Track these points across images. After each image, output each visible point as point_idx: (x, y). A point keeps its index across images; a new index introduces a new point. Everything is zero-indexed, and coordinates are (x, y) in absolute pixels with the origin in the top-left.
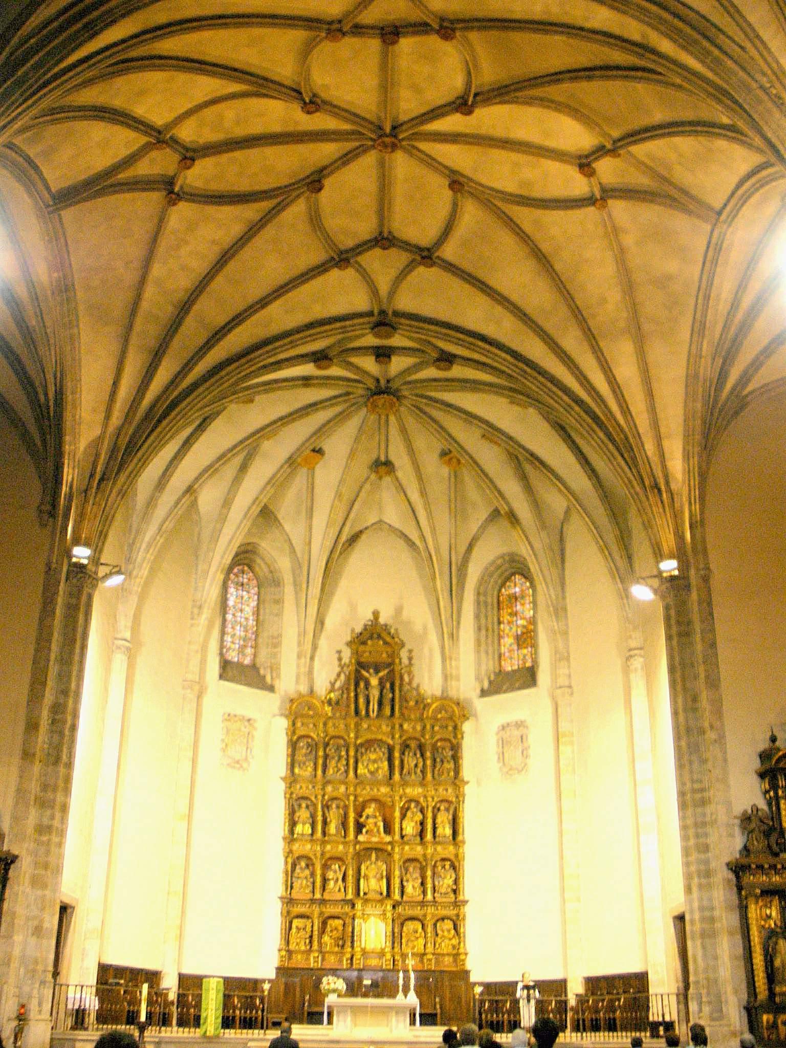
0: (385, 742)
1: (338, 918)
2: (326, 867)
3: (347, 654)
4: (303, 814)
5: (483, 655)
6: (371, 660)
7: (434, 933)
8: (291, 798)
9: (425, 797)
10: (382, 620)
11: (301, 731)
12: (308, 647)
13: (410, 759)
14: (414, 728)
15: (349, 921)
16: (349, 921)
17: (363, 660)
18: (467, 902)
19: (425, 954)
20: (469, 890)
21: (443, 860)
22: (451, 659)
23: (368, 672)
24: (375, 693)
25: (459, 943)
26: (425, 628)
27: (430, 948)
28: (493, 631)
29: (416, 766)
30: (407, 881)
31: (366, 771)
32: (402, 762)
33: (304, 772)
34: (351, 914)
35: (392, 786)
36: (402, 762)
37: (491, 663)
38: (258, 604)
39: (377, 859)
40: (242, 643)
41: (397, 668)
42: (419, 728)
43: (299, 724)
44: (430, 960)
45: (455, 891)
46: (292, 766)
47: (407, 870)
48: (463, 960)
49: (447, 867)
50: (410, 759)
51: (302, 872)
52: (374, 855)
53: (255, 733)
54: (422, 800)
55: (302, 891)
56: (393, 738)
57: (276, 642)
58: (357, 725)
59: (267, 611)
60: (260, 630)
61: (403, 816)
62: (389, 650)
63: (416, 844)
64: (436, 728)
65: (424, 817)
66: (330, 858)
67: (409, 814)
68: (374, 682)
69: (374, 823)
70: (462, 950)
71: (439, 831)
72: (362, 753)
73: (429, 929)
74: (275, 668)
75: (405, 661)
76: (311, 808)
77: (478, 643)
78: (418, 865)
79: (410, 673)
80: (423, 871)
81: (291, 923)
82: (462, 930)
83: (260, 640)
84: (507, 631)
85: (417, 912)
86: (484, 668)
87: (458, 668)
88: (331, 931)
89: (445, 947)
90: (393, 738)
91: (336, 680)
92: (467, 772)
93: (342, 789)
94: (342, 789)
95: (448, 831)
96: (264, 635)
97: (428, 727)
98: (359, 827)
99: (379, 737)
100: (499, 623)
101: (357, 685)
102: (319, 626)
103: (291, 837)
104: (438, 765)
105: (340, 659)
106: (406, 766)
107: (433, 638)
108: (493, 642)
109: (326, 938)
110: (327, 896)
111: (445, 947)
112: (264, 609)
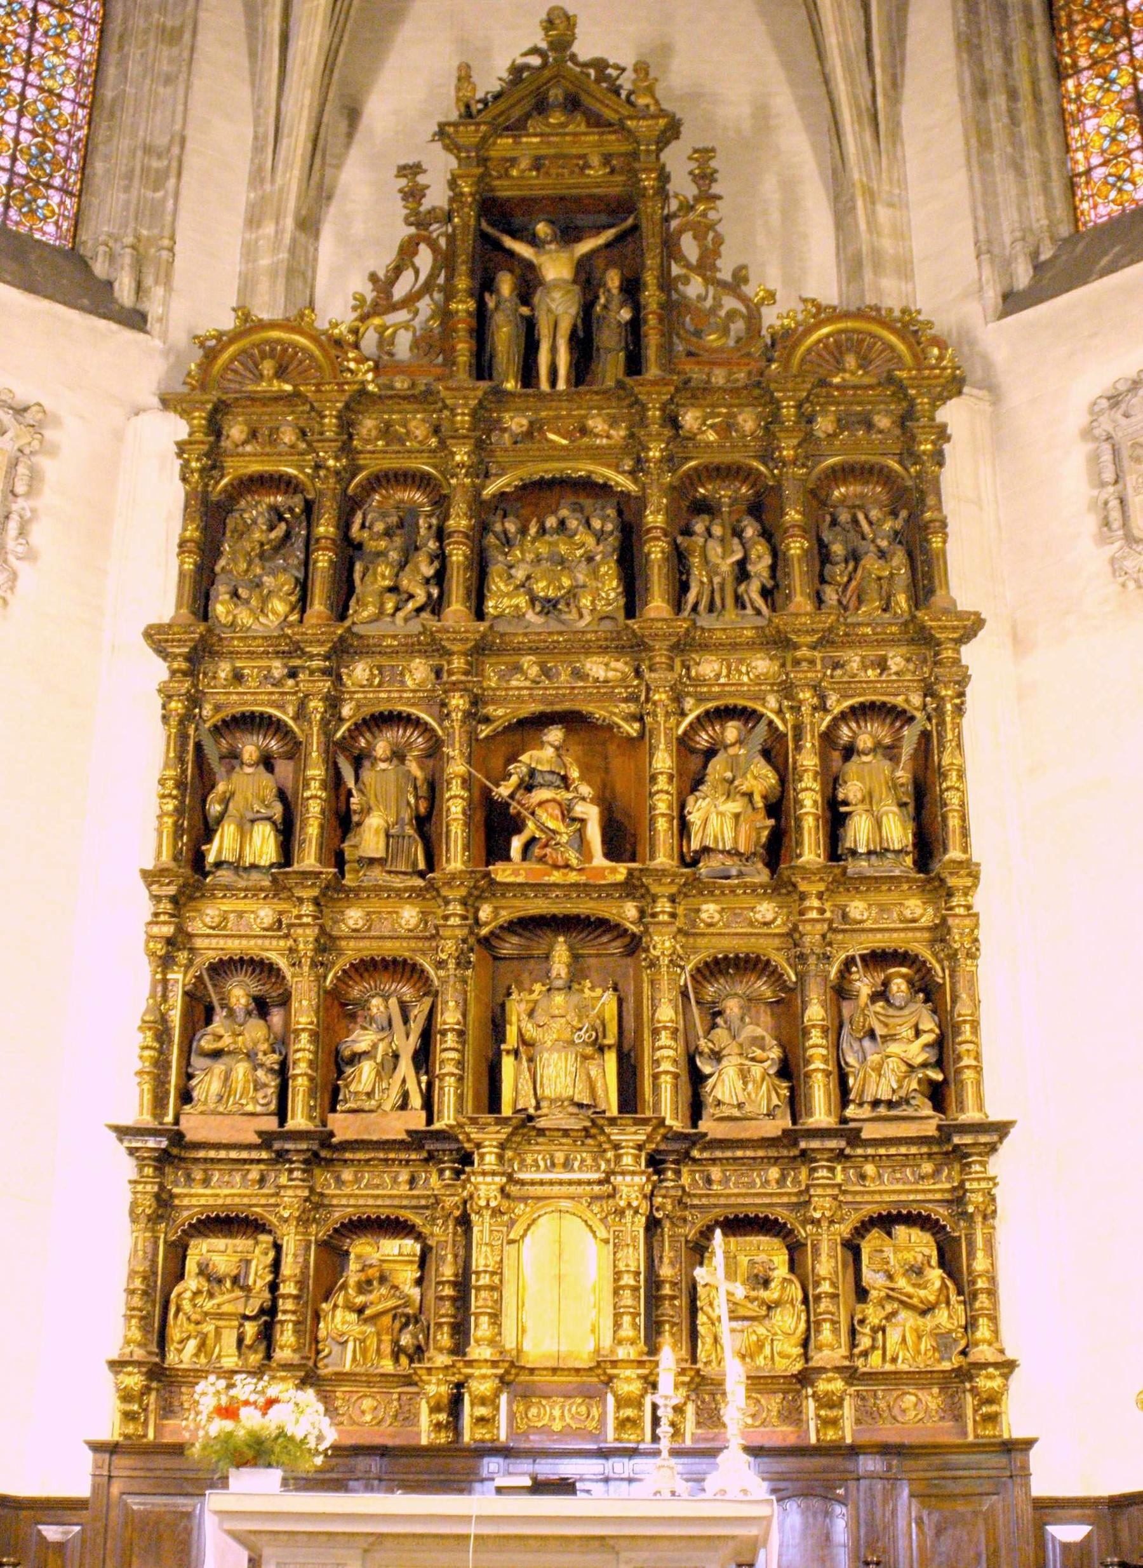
0: (604, 489)
1: (396, 1227)
2: (340, 1008)
3: (440, 170)
4: (246, 787)
5: (1005, 182)
6: (539, 185)
7: (846, 1289)
8: (186, 719)
9: (787, 690)
10: (585, 48)
11: (249, 463)
12: (291, 178)
13: (715, 550)
14: (727, 428)
15: (441, 1233)
16: (441, 1233)
17: (505, 190)
18: (1002, 1129)
19: (805, 1378)
20: (998, 1085)
21: (878, 959)
22: (871, 197)
23: (533, 241)
24: (559, 308)
25: (970, 1325)
26: (762, 115)
27: (831, 1350)
28: (1037, 98)
29: (742, 572)
30: (717, 1056)
31: (522, 601)
32: (679, 559)
33: (258, 612)
34: (449, 1202)
35: (635, 648)
36: (679, 559)
37: (1037, 202)
38: (100, 58)
39: (577, 974)
40: (21, 168)
41: (650, 209)
42: (747, 421)
43: (236, 431)
44: (831, 1402)
45: (937, 1095)
46: (200, 590)
47: (714, 1014)
48: (992, 1399)
49: (899, 987)
50: (715, 550)
51: (236, 1030)
52: (561, 953)
53: (45, 463)
54: (769, 706)
55: (229, 1101)
56: (639, 467)
57: (163, 165)
58: (484, 423)
59: (134, 69)
60: (102, 133)
61: (692, 782)
62: (614, 143)
63: (753, 889)
64: (824, 425)
65: (783, 781)
66: (368, 967)
67: (717, 768)
68: (556, 267)
69: (564, 813)
70: (983, 1353)
71: (859, 832)
72: (508, 541)
73: (826, 1264)
74: (152, 258)
75: (682, 186)
76: (284, 768)
77: (980, 138)
78: (762, 987)
79: (702, 230)
80: (786, 1006)
81: (178, 1251)
82: (980, 1263)
83: (99, 167)
84: (1092, 94)
85: (764, 1188)
86: (1009, 220)
87: (901, 233)
88: (364, 1286)
89: (905, 1342)
90: (640, 464)
91: (398, 271)
92: (965, 583)
93: (419, 671)
94: (419, 671)
95: (898, 832)
96: (117, 152)
97: (788, 411)
98: (496, 826)
99: (582, 468)
100: (1060, 74)
101: (485, 285)
102: (334, 121)
103: (190, 872)
104: (839, 573)
105: (413, 194)
106: (698, 576)
107: (797, 146)
108: (1040, 133)
109: (338, 1321)
110: (343, 1126)
111: (905, 1342)
112: (122, 62)
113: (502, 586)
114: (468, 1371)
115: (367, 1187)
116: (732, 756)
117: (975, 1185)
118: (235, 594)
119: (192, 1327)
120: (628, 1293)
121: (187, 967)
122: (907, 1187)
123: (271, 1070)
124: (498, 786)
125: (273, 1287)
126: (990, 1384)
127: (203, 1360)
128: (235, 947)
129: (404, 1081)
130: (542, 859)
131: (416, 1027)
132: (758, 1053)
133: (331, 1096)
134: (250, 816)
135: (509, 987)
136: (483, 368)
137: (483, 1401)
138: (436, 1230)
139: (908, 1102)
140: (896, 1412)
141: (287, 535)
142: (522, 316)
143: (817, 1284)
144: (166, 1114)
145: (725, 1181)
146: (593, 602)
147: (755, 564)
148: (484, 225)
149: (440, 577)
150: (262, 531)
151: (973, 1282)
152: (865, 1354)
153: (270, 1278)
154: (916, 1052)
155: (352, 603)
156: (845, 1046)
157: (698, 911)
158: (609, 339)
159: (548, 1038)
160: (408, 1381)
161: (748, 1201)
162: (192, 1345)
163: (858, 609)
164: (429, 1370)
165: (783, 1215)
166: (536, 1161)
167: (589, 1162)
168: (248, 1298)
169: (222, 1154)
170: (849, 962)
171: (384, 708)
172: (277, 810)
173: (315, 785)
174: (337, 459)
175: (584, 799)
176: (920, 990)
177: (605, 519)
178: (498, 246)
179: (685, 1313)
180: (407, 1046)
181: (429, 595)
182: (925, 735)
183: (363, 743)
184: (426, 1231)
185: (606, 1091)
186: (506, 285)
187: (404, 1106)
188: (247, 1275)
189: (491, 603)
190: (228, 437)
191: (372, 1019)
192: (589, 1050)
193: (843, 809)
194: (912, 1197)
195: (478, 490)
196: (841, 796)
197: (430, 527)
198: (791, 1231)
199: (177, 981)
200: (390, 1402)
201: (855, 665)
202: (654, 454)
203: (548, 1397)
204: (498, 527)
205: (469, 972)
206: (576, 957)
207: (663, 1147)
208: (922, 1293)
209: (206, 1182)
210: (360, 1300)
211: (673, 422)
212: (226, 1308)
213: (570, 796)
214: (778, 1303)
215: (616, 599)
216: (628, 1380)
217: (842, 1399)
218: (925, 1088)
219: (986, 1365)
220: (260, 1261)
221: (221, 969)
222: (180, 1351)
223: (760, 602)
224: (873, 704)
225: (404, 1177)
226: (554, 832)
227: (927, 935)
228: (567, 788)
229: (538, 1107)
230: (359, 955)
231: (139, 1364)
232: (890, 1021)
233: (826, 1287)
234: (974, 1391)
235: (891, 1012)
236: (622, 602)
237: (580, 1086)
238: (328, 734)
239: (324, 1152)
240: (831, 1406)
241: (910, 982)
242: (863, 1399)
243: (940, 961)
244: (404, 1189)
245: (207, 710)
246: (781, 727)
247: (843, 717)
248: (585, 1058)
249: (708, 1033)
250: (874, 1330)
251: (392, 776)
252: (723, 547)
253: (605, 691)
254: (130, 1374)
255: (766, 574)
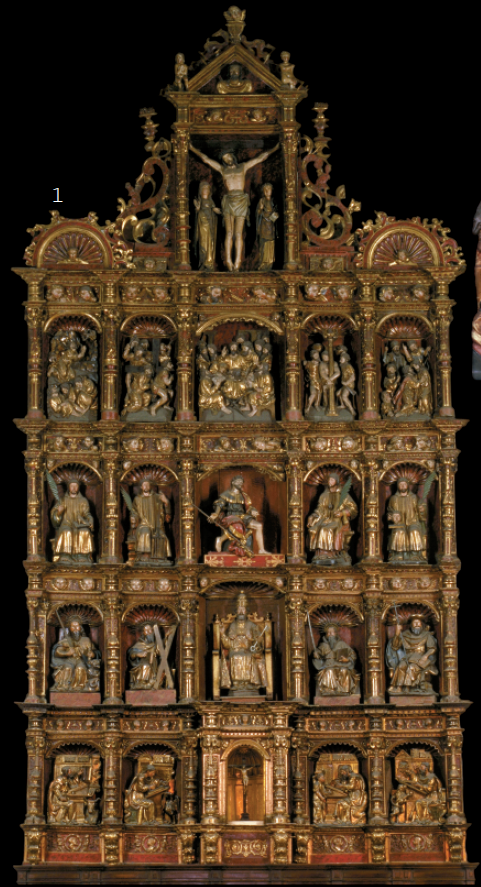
1: (161, 748)
2: (130, 631)
13: (325, 370)
15: (186, 754)
16: (186, 754)
21: (407, 607)
23: (221, 162)
24: (237, 211)
29: (339, 384)
39: (251, 609)
47: (322, 634)
49: (417, 624)
50: (325, 370)
52: (242, 602)
58: (199, 291)
63: (343, 571)
64: (386, 294)
66: (142, 609)
68: (235, 183)
69: (246, 532)
72: (209, 357)
85: (349, 731)
88: (147, 781)
95: (418, 541)
110: (134, 699)
113: (208, 390)
114: (203, 830)
115: (147, 728)
116: (331, 493)
117: (452, 733)
118: (61, 392)
119: (61, 803)
120: (280, 790)
121: (48, 611)
122: (418, 731)
123: (96, 668)
124: (210, 515)
125: (101, 781)
126: (456, 835)
127: (67, 820)
128: (72, 599)
129: (164, 672)
130: (232, 552)
131: (168, 644)
132: (345, 659)
133: (127, 681)
134: (77, 525)
135: (215, 616)
136: (195, 260)
137: (211, 844)
138: (183, 752)
139: (419, 687)
140: (411, 845)
141: (87, 354)
142: (217, 215)
143: (373, 782)
144: (42, 691)
145: (327, 727)
146: (258, 401)
147: (346, 381)
148: (191, 146)
149: (174, 385)
150: (74, 353)
151: (450, 782)
152: (397, 816)
153: (99, 777)
154: (425, 660)
155: (126, 399)
156: (389, 654)
157: (314, 581)
158: (266, 232)
159: (236, 647)
160: (171, 830)
161: (338, 737)
162: (61, 811)
163: (401, 407)
164: (183, 828)
165: (355, 744)
166: (233, 719)
167: (260, 720)
168: (89, 787)
169: (73, 713)
170: (391, 611)
171: (146, 463)
172: (91, 522)
173: (112, 511)
174: (114, 313)
175: (254, 518)
176: (428, 623)
177: (264, 345)
178: (200, 160)
179: (307, 794)
180: (165, 654)
181: (168, 395)
182: (436, 483)
183: (134, 479)
184: (177, 751)
185: (266, 677)
186: (205, 191)
187: (163, 685)
188: (87, 775)
189: (202, 401)
190: (51, 294)
191: (145, 637)
192: (257, 655)
193: (391, 527)
194: (421, 735)
195: (193, 331)
196: (389, 518)
197: (167, 350)
198: (360, 752)
199: (43, 618)
200: (162, 840)
201: (399, 443)
202: (292, 315)
203: (241, 840)
204: (205, 352)
205: (196, 614)
206: (249, 600)
207: (297, 712)
208: (425, 787)
209: (64, 727)
210: (145, 788)
211: (302, 289)
212: (78, 794)
213: (247, 517)
214: (353, 790)
215: (270, 399)
216: (281, 834)
217: (384, 841)
218: (429, 678)
219: (454, 826)
220: (94, 768)
221: (65, 610)
222: (55, 816)
223: (349, 404)
224: (408, 464)
225: (166, 724)
226: (239, 539)
227: (432, 596)
228: (245, 513)
229: (232, 685)
230: (139, 604)
231: (38, 826)
232: (413, 642)
233: (377, 783)
234: (450, 838)
235: (413, 637)
236: (273, 401)
237: (254, 674)
238: (116, 479)
239: (127, 712)
240: (379, 844)
241: (422, 620)
242: (395, 839)
243: (438, 610)
244: (166, 731)
245: (50, 463)
246: (359, 478)
247: (392, 470)
248: (256, 658)
249: (318, 646)
250: (401, 804)
251: (151, 499)
252: (329, 369)
253: (265, 456)
254: (34, 831)
255: (352, 386)
